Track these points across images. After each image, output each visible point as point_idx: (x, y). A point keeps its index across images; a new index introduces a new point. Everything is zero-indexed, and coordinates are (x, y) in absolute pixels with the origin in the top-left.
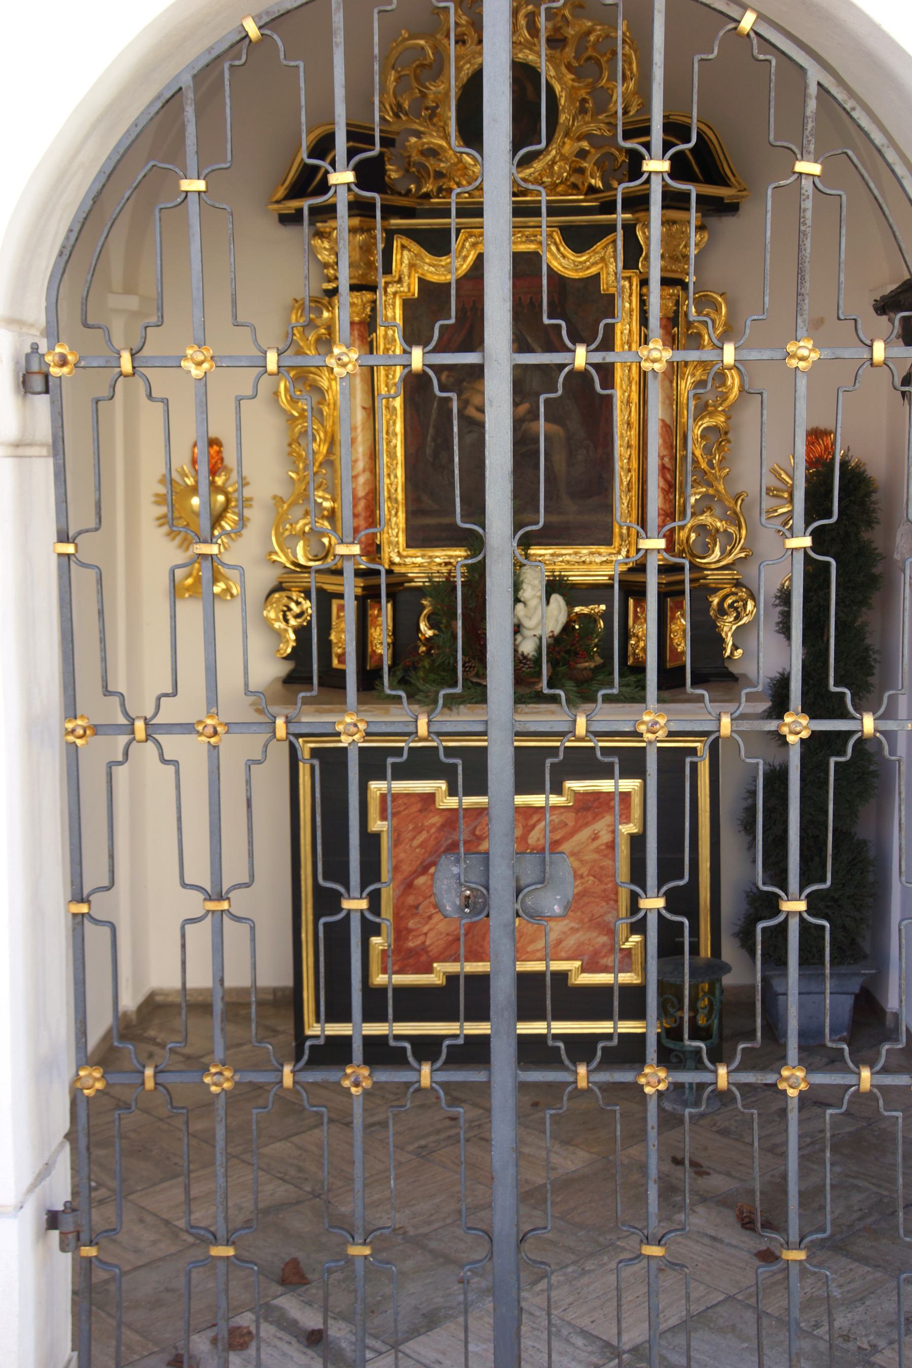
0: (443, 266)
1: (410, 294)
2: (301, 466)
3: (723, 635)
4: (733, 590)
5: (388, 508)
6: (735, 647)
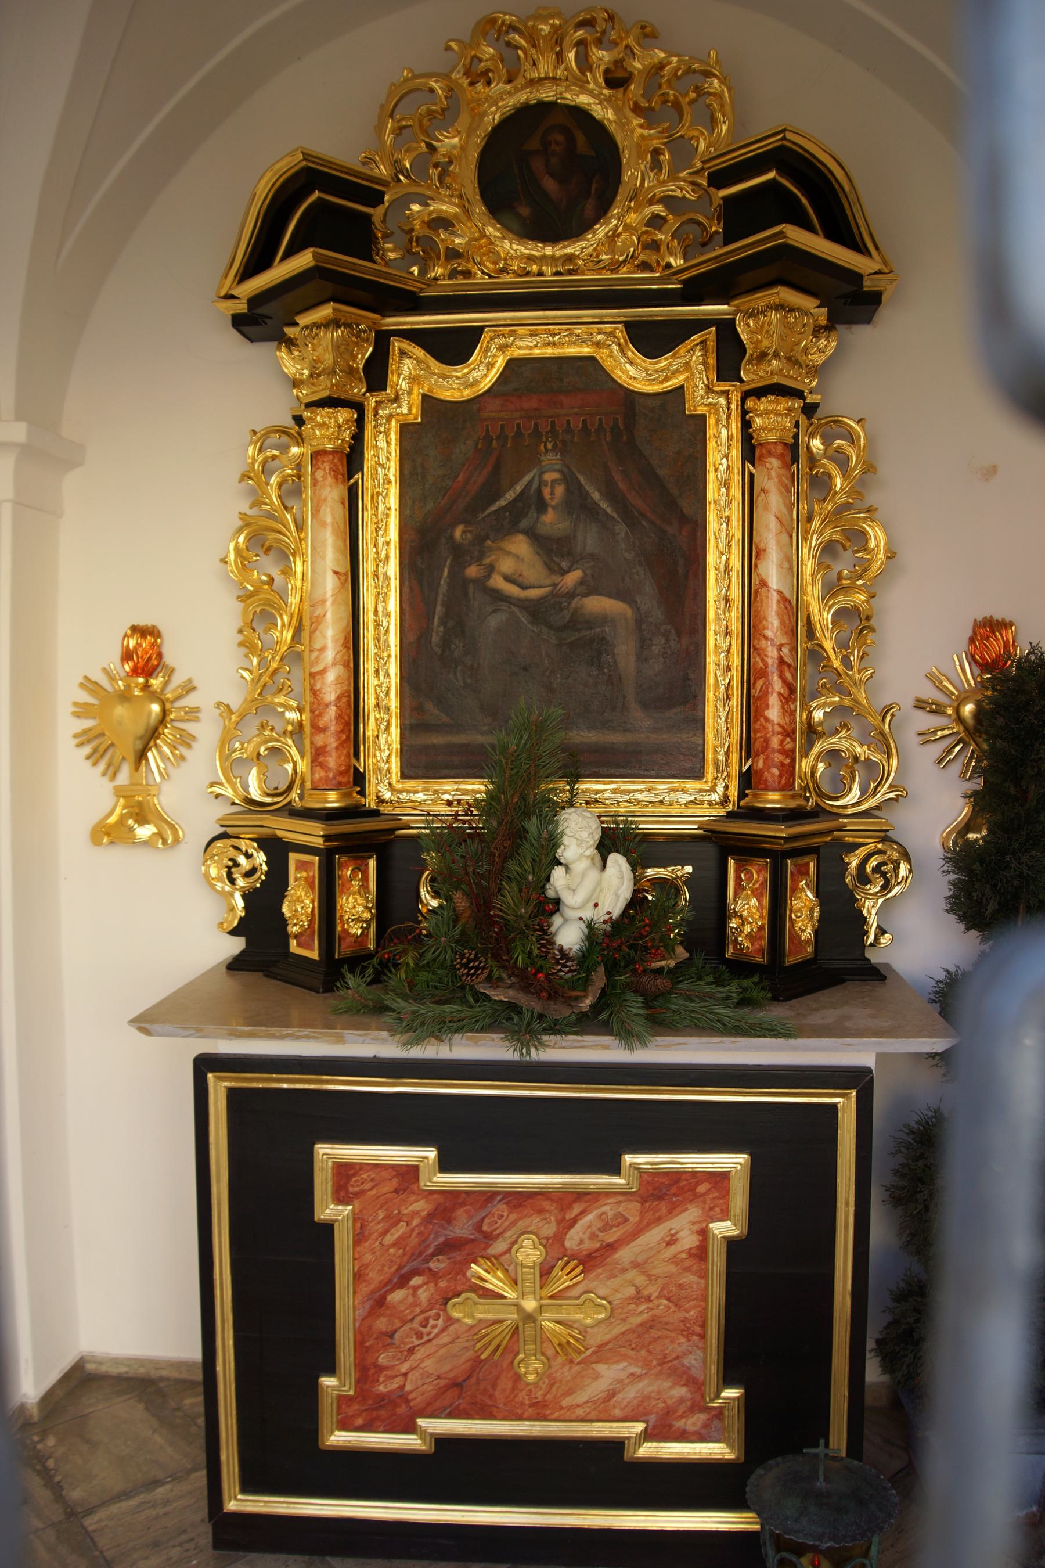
0: (458, 378)
1: (411, 417)
2: (255, 661)
3: (865, 912)
4: (880, 846)
5: (376, 720)
6: (881, 931)
